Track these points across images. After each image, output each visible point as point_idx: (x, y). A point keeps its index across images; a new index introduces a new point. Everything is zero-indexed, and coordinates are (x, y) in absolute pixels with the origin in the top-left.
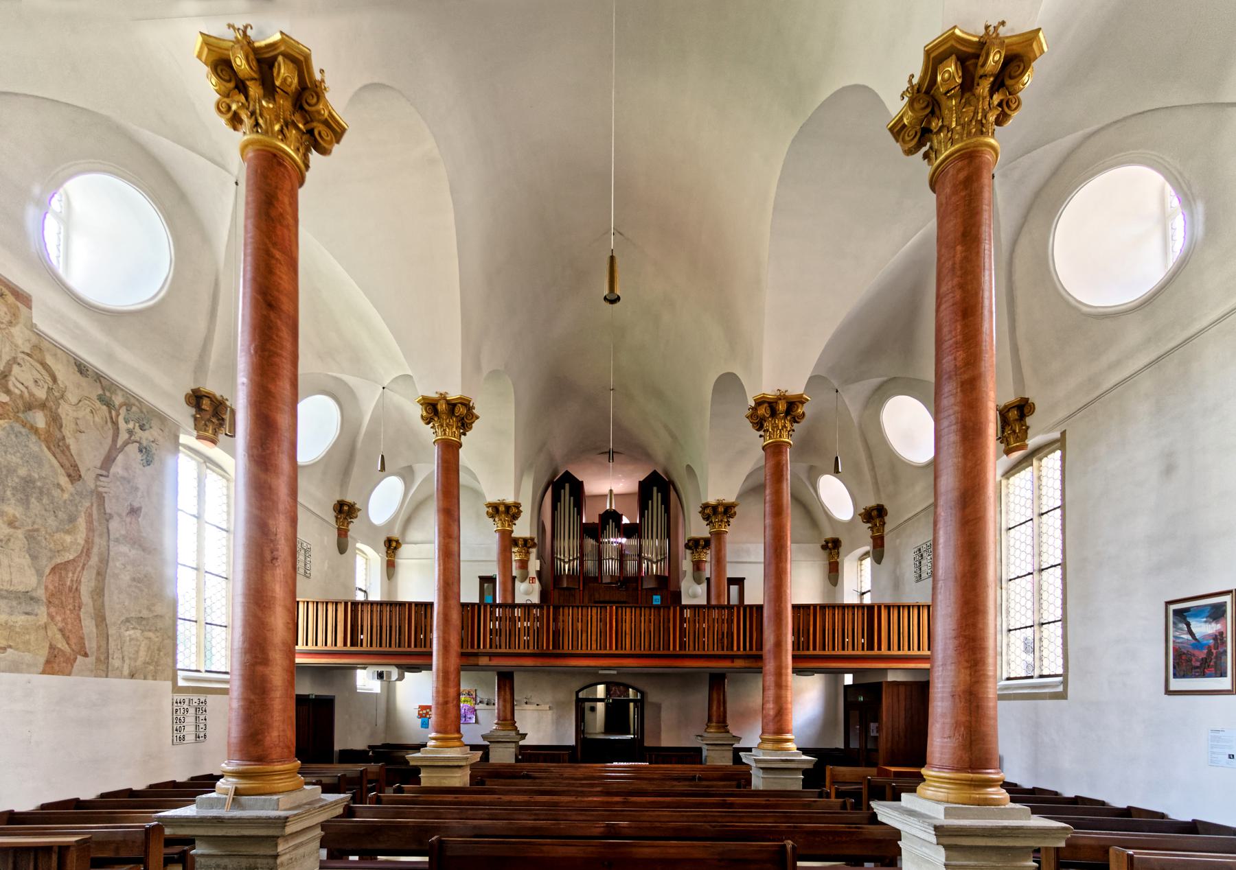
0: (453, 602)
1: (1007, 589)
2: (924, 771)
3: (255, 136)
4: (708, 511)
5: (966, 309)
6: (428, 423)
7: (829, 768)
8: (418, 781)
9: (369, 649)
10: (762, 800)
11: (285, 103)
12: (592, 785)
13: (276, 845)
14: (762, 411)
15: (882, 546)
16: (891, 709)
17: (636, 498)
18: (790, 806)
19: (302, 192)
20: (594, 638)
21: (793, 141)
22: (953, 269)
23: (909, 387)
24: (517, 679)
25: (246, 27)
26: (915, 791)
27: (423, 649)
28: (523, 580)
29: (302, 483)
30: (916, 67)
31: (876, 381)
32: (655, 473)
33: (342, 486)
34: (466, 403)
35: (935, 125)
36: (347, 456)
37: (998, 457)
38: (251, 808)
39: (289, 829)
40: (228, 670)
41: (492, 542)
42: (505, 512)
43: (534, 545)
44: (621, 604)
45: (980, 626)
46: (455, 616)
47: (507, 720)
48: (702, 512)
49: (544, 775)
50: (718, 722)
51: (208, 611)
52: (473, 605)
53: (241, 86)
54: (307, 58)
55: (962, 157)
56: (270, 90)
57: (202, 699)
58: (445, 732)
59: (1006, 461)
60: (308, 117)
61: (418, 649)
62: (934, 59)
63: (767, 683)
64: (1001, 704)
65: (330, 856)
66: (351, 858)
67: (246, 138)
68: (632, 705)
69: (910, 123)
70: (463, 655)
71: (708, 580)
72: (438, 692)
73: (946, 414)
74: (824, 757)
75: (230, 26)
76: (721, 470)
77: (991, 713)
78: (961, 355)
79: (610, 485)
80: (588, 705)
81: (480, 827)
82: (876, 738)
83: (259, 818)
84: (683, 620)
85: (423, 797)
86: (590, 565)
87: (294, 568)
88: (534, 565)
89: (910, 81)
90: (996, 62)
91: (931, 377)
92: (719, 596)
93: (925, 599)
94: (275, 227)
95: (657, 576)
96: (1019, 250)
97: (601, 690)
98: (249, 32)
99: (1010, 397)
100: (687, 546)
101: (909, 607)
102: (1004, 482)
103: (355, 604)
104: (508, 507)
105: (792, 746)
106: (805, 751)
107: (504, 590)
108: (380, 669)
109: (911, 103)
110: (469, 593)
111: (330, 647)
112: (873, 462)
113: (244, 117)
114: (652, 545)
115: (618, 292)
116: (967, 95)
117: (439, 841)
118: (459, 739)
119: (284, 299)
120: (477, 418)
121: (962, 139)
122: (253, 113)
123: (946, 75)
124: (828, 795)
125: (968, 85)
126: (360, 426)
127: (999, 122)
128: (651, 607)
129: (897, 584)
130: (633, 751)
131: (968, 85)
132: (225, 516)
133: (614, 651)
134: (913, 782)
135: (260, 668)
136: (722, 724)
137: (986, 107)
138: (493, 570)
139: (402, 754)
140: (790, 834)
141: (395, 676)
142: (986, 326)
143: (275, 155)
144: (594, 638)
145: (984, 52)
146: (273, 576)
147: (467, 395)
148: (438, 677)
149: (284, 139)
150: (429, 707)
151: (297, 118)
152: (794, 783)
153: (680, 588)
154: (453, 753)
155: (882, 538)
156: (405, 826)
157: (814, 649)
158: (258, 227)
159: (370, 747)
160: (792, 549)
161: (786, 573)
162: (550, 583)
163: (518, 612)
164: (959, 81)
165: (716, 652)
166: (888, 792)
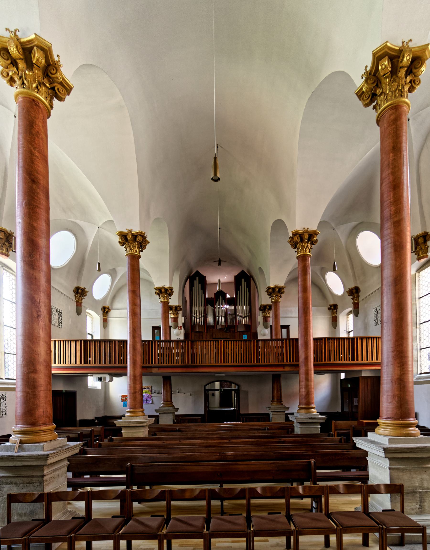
0: (138, 340)
1: (420, 328)
2: (378, 421)
3: (22, 90)
4: (270, 291)
5: (396, 186)
6: (123, 245)
7: (333, 422)
8: (121, 435)
9: (94, 365)
10: (299, 439)
11: (38, 73)
12: (213, 434)
13: (43, 470)
14: (296, 239)
15: (358, 307)
16: (363, 390)
17: (233, 285)
18: (315, 442)
19: (49, 121)
20: (212, 357)
21: (309, 99)
22: (389, 164)
23: (369, 227)
24: (173, 380)
25: (16, 31)
26: (374, 431)
27: (122, 365)
28: (175, 327)
29: (54, 277)
30: (369, 62)
31: (353, 224)
32: (243, 272)
33: (78, 280)
34: (142, 235)
35: (378, 92)
36: (80, 264)
37: (412, 263)
38: (29, 450)
39: (50, 461)
40: (15, 378)
41: (158, 308)
42: (165, 292)
43: (181, 310)
44: (226, 339)
45: (405, 345)
46: (139, 347)
47: (168, 401)
48: (267, 291)
49: (188, 429)
50: (277, 400)
51: (6, 346)
52: (149, 341)
53: (14, 62)
54: (50, 48)
55: (391, 108)
56: (30, 65)
57: (4, 394)
58: (135, 408)
59: (418, 264)
60: (52, 81)
61: (120, 365)
62: (377, 58)
63: (301, 379)
64: (416, 387)
65: (74, 476)
66: (86, 476)
67: (18, 90)
68: (233, 392)
69: (366, 90)
70: (143, 367)
71: (271, 326)
72: (130, 387)
73: (386, 238)
74: (331, 416)
75: (7, 29)
76: (277, 269)
77: (411, 389)
78: (393, 208)
79: (220, 278)
80: (211, 392)
81: (153, 458)
82: (357, 406)
83: (33, 456)
84: (258, 347)
85: (124, 443)
86: (210, 319)
87: (50, 321)
88: (181, 320)
89: (366, 69)
90: (408, 60)
91: (379, 221)
92: (276, 334)
93: (378, 334)
94: (34, 139)
95: (245, 324)
96: (423, 157)
97: (217, 385)
98: (17, 33)
99: (418, 231)
100: (260, 309)
101: (372, 338)
102: (417, 274)
103: (86, 341)
104: (166, 290)
105: (314, 410)
106: (321, 414)
107: (165, 333)
108: (100, 376)
109: (366, 81)
110: (147, 335)
111: (73, 365)
112: (353, 265)
113: (16, 79)
114: (242, 309)
115: (219, 175)
116: (394, 77)
117: (131, 465)
118: (142, 412)
119: (40, 177)
120: (149, 243)
121: (391, 99)
122: (21, 77)
123: (383, 66)
124: (333, 436)
125: (394, 72)
126: (87, 247)
127: (410, 91)
128: (242, 340)
129: (366, 326)
130: (234, 416)
131: (394, 72)
132: (14, 295)
133: (223, 364)
134: (373, 427)
135: (32, 375)
136: (279, 400)
137: (403, 83)
138: (159, 323)
139: (112, 421)
140: (313, 456)
141: (108, 379)
142: (405, 194)
143: (34, 100)
144: (212, 357)
145: (402, 55)
146: (38, 325)
147: (143, 231)
148: (130, 379)
149: (39, 91)
150: (126, 396)
151: (45, 81)
152: (316, 430)
153: (257, 331)
154: (139, 419)
155: (358, 304)
156: (114, 458)
157: (325, 361)
158: (25, 138)
159: (96, 418)
160: (312, 310)
161: (310, 322)
162: (189, 328)
163: (173, 345)
164: (390, 69)
165: (275, 363)
166: (363, 433)
